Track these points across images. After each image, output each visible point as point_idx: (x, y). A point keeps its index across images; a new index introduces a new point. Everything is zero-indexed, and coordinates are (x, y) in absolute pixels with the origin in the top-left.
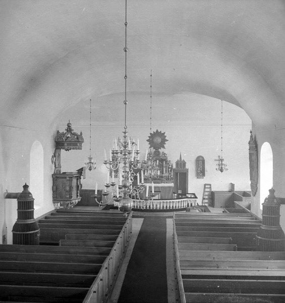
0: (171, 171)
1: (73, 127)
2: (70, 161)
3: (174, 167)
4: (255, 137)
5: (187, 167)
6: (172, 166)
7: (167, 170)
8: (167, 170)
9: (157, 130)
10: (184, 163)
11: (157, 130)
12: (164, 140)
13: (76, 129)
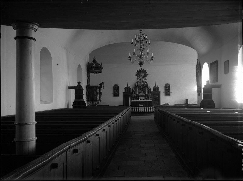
2: (96, 80)
3: (152, 90)
4: (200, 63)
5: (159, 90)
6: (151, 90)
7: (148, 92)
8: (148, 92)
9: (146, 70)
10: (158, 88)
11: (146, 70)
12: (146, 75)
13: (99, 62)
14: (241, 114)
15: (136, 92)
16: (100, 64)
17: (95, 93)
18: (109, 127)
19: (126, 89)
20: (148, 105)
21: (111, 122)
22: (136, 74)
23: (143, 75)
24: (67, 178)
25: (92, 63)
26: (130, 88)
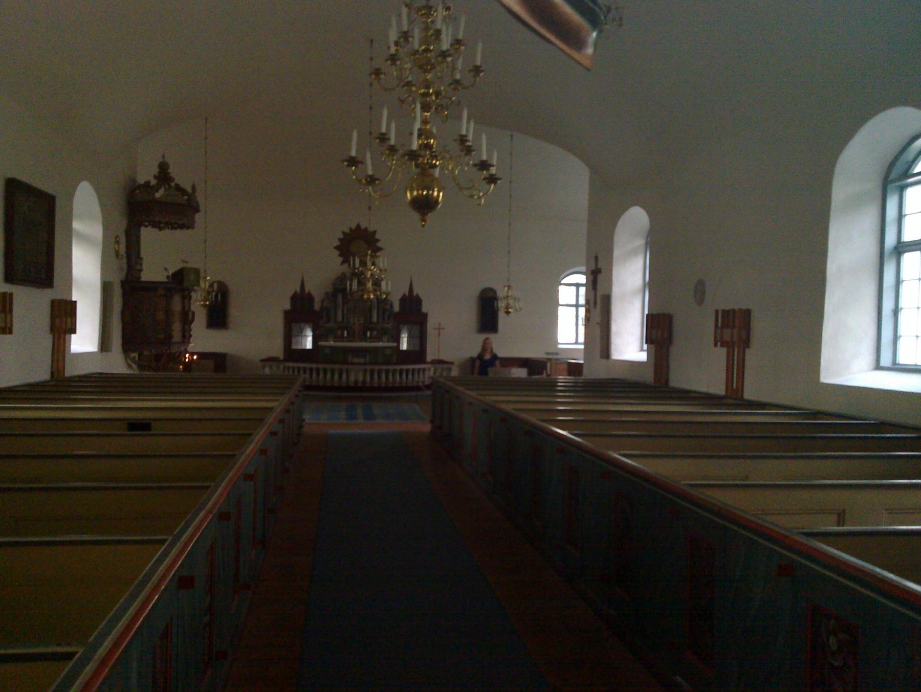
1: (173, 171)
19: (294, 298)
26: (310, 298)
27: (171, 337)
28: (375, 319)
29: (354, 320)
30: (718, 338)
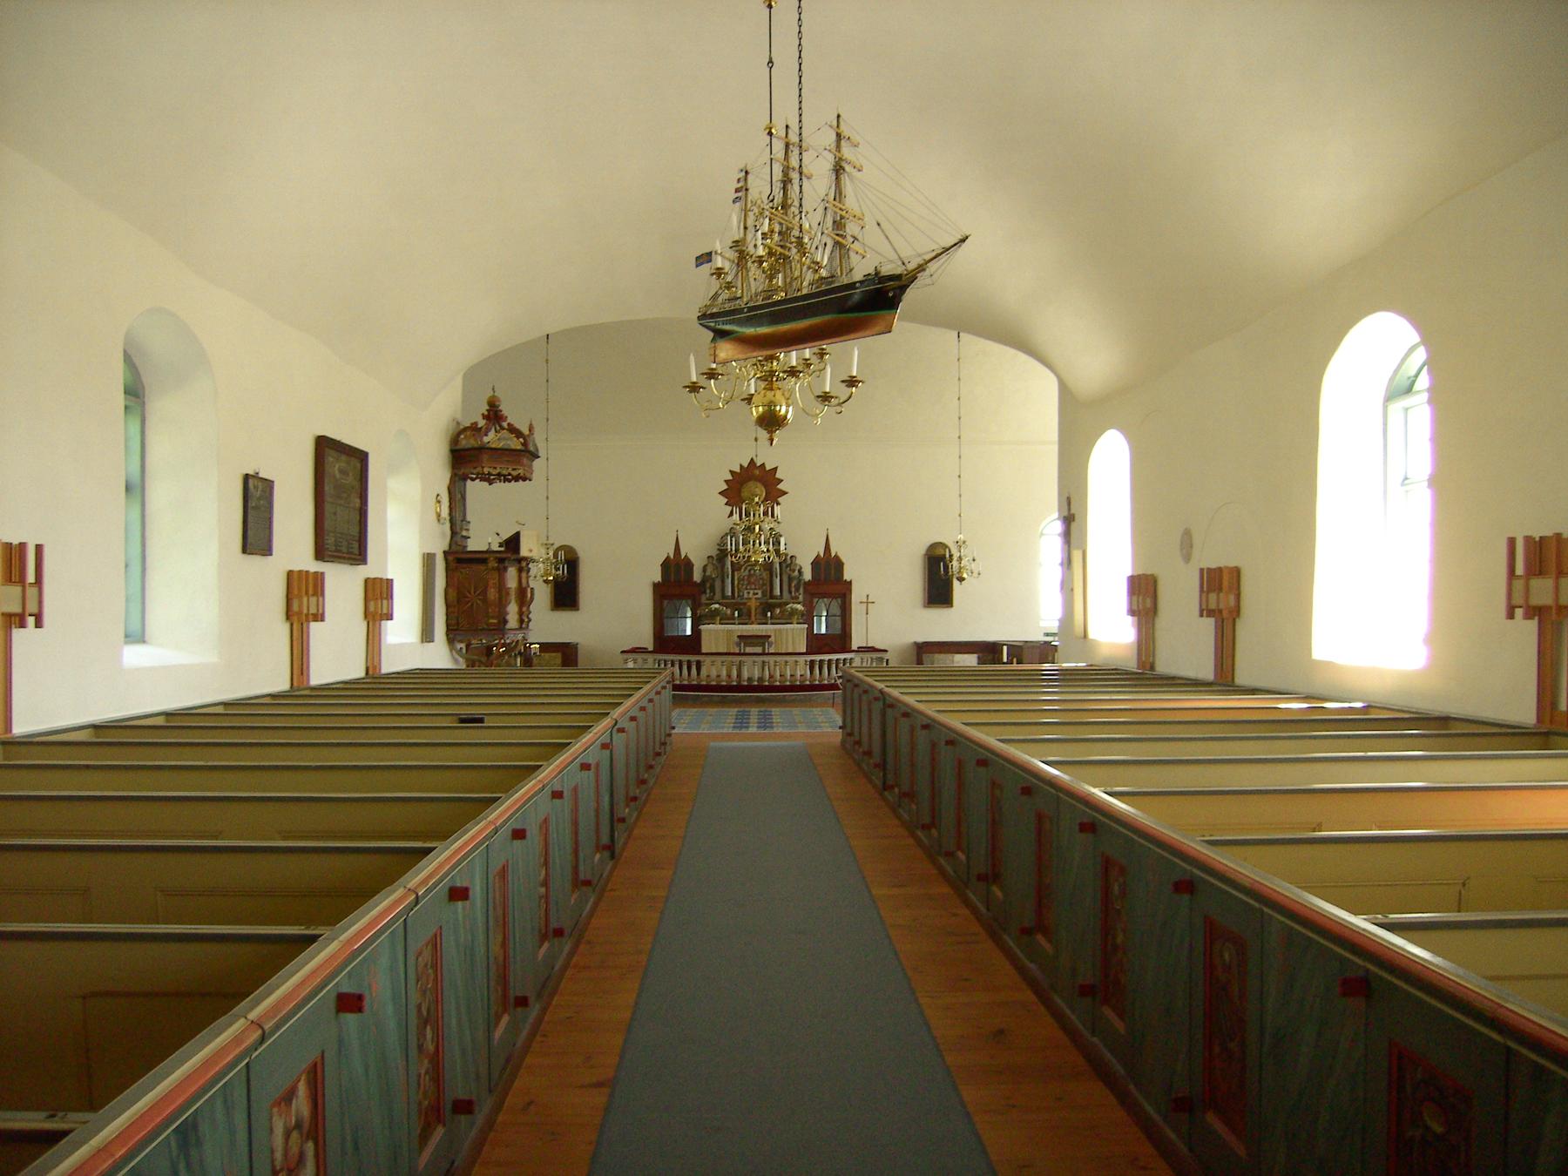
0: (797, 590)
1: (505, 408)
6: (800, 572)
14: (784, 647)
15: (723, 582)
16: (526, 432)
17: (492, 594)
18: (641, 710)
19: (666, 565)
20: (450, 610)
21: (654, 691)
22: (725, 487)
23: (760, 491)
24: (504, 897)
25: (482, 423)
26: (688, 564)
27: (506, 622)
28: (777, 592)
29: (749, 593)
30: (32, 592)
